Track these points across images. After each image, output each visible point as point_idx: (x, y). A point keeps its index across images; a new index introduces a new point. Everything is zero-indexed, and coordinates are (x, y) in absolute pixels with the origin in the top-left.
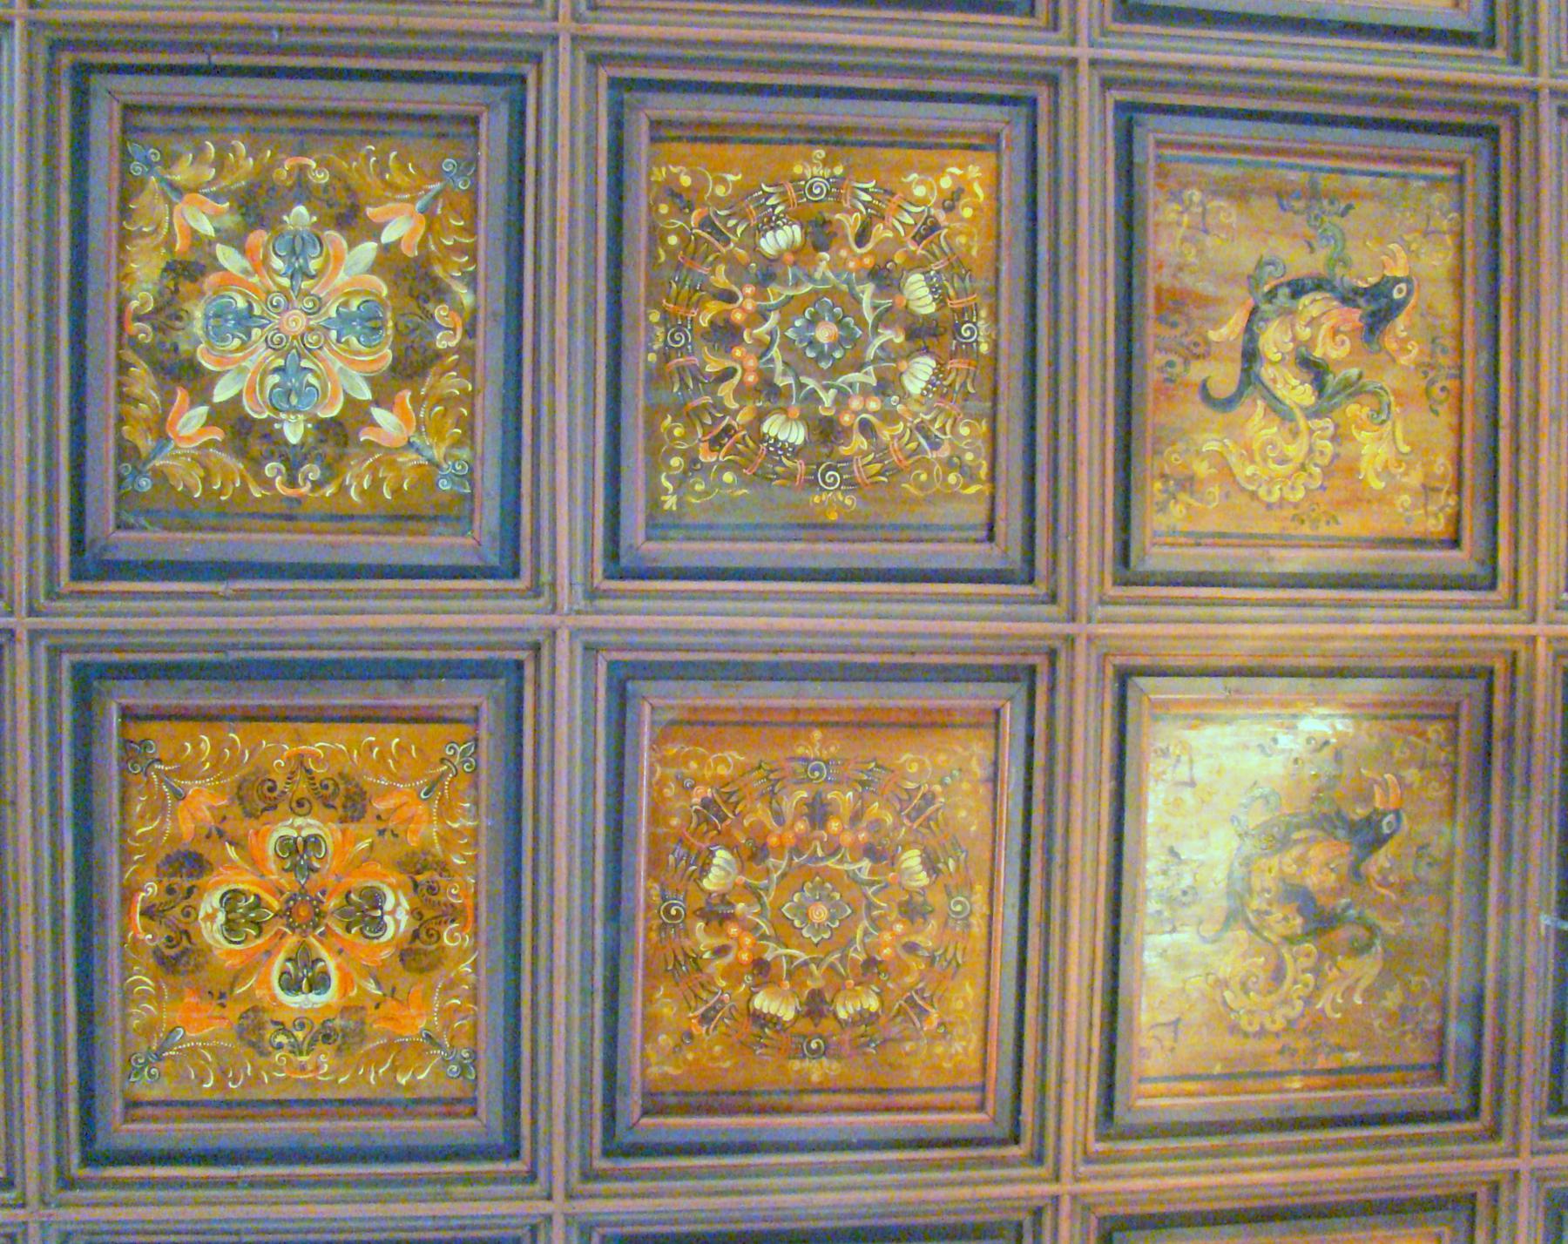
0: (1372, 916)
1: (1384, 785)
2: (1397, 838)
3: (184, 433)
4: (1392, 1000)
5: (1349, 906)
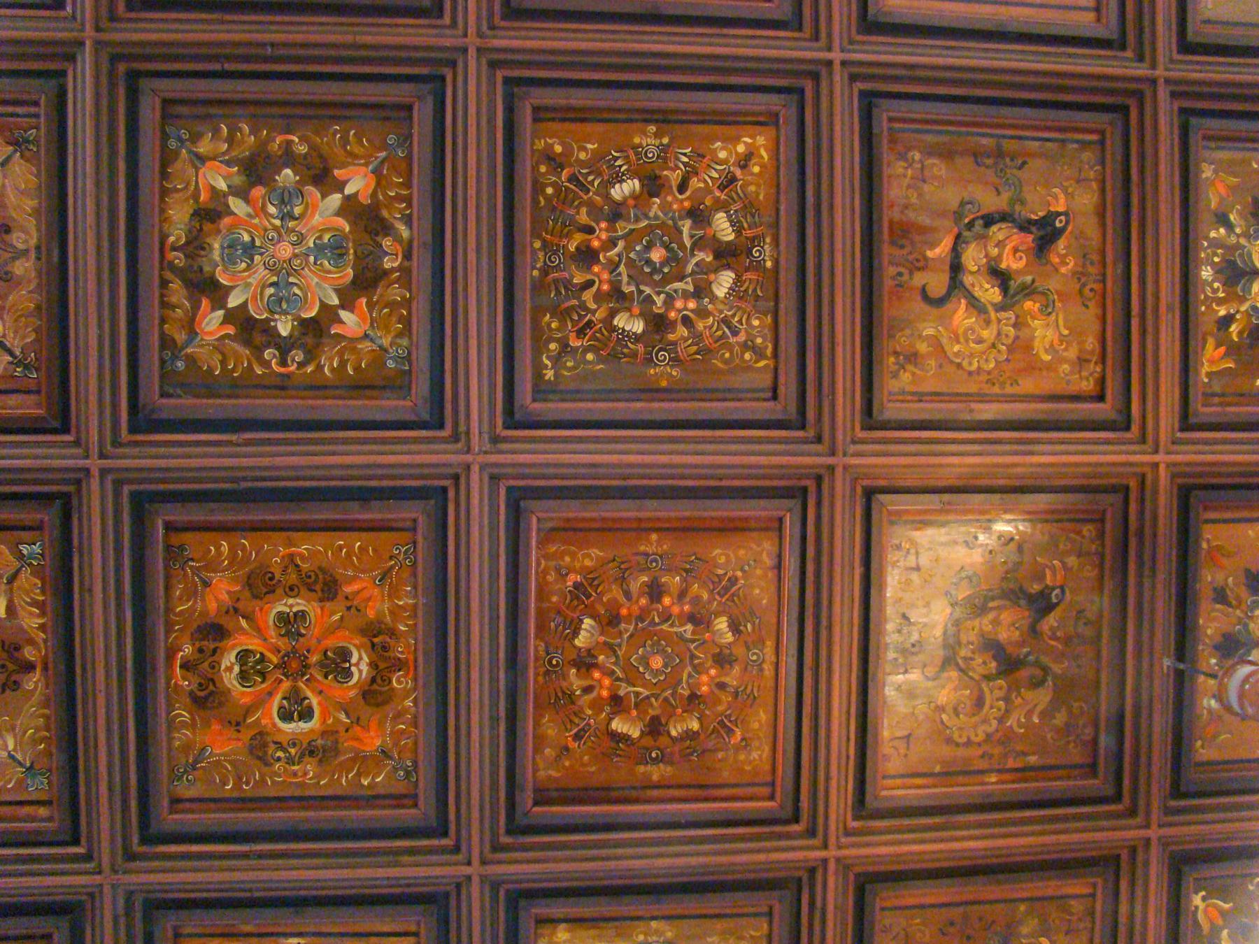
0: (1045, 660)
1: (1053, 569)
2: (1062, 606)
4: (1060, 719)
5: (1029, 654)
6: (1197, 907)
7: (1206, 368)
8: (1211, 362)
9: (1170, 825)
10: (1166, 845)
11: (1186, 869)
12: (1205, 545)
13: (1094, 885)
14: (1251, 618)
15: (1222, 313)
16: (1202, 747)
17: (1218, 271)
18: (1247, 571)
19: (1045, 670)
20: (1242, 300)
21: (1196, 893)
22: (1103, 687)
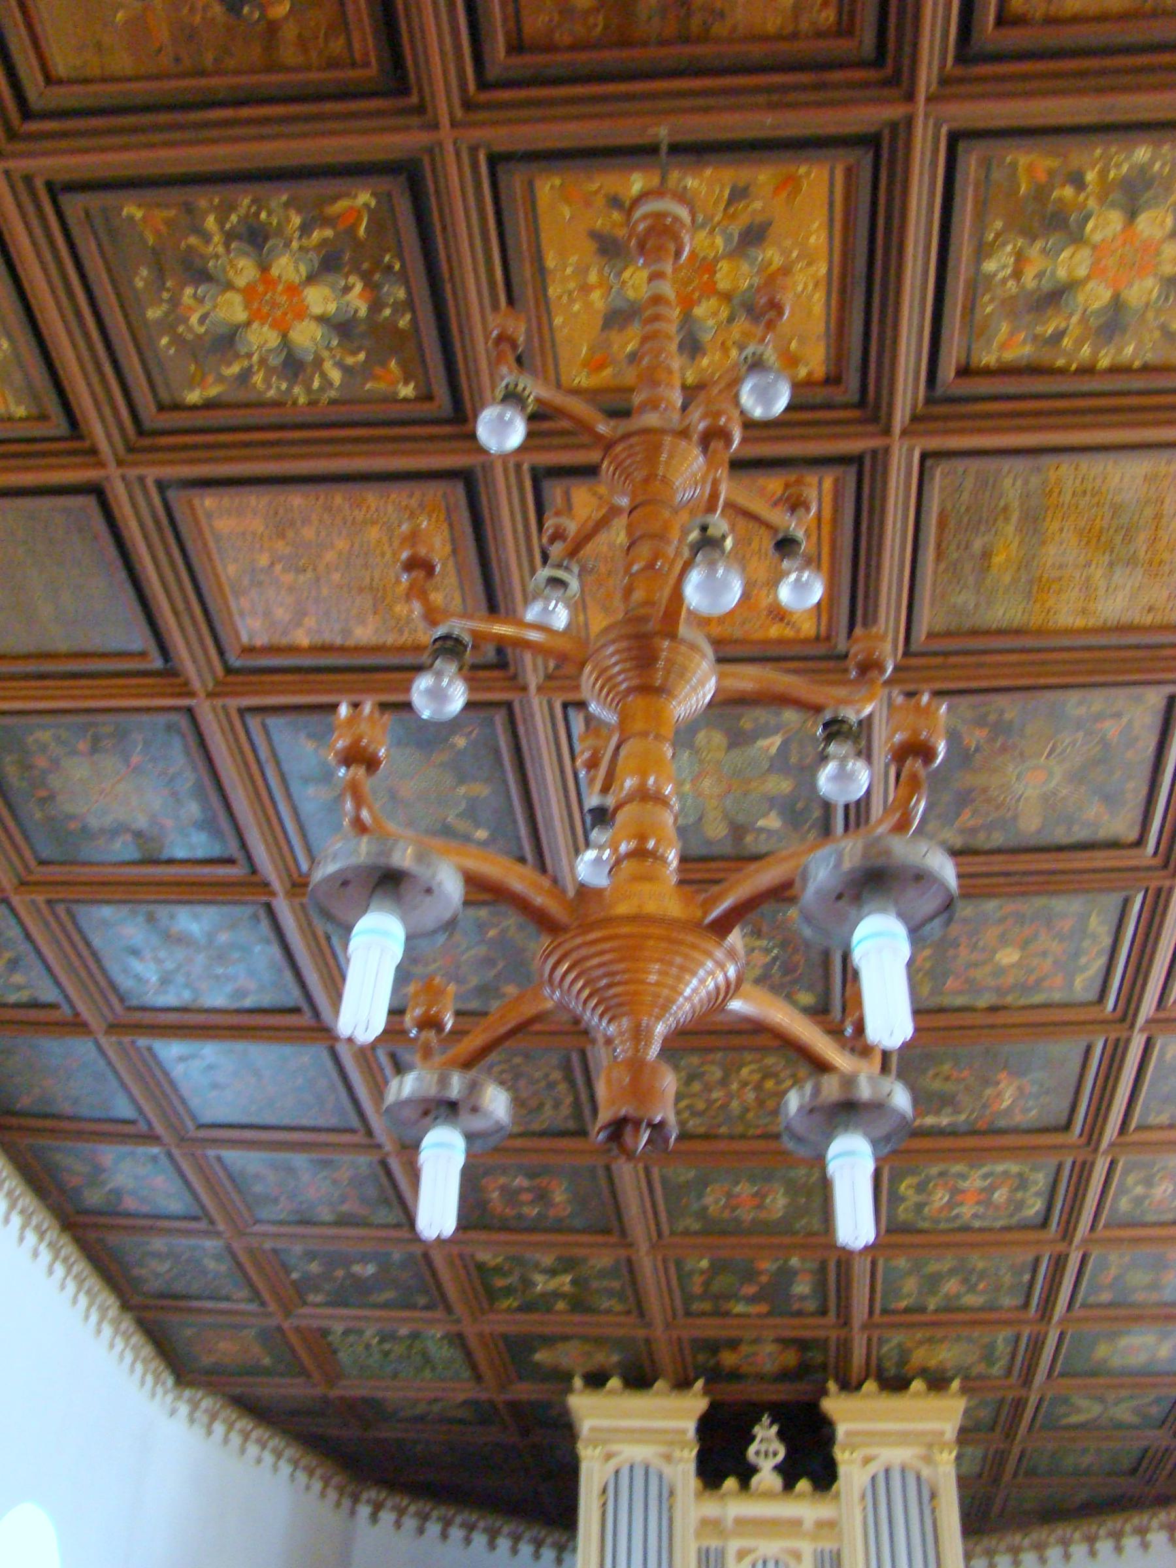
7: (1023, 160)
8: (1030, 168)
9: (458, 153)
10: (430, 151)
11: (402, 179)
12: (802, 170)
13: (367, 65)
14: (711, 232)
17: (1143, 170)
18: (770, 224)
20: (1102, 199)
21: (374, 194)
22: (625, 54)
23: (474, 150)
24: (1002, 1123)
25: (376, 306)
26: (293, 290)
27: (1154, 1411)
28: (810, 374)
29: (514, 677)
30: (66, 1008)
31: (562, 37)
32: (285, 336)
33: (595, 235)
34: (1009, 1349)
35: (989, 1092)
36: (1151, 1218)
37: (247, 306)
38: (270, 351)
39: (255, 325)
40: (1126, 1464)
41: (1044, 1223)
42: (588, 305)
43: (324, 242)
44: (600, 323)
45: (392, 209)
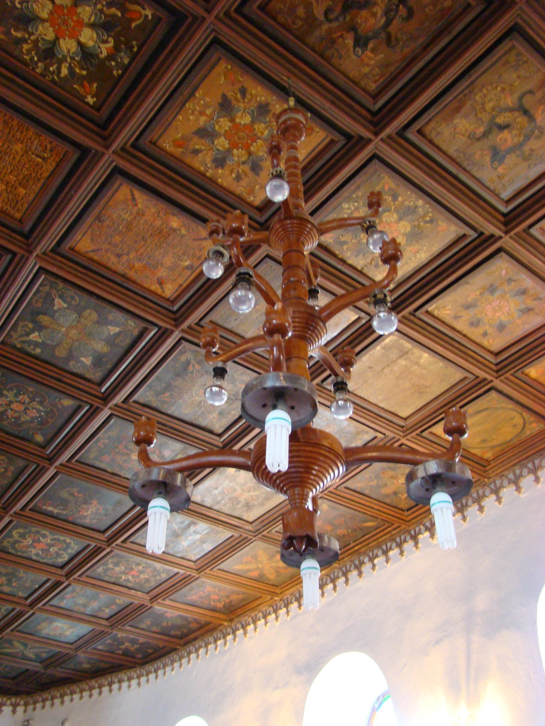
0: (335, 24)
1: (371, 59)
2: (352, 49)
3: (62, 401)
4: (301, 11)
5: (345, 18)
6: (144, 9)
12: (317, 130)
14: (267, 128)
15: (400, 199)
16: (226, 67)
19: (329, 21)
21: (152, 15)
23: (213, 30)
24: (79, 521)
25: (111, 57)
26: (80, 23)
27: (44, 655)
28: (254, 201)
29: (29, 245)
30: (380, 435)
31: (281, 18)
32: (57, 39)
33: (224, 97)
34: (5, 614)
35: (84, 506)
36: (106, 579)
37: (51, 13)
38: (43, 39)
39: (47, 24)
40: (14, 674)
41: (62, 567)
42: (197, 120)
43: (114, 16)
44: (194, 129)
45: (155, 27)
